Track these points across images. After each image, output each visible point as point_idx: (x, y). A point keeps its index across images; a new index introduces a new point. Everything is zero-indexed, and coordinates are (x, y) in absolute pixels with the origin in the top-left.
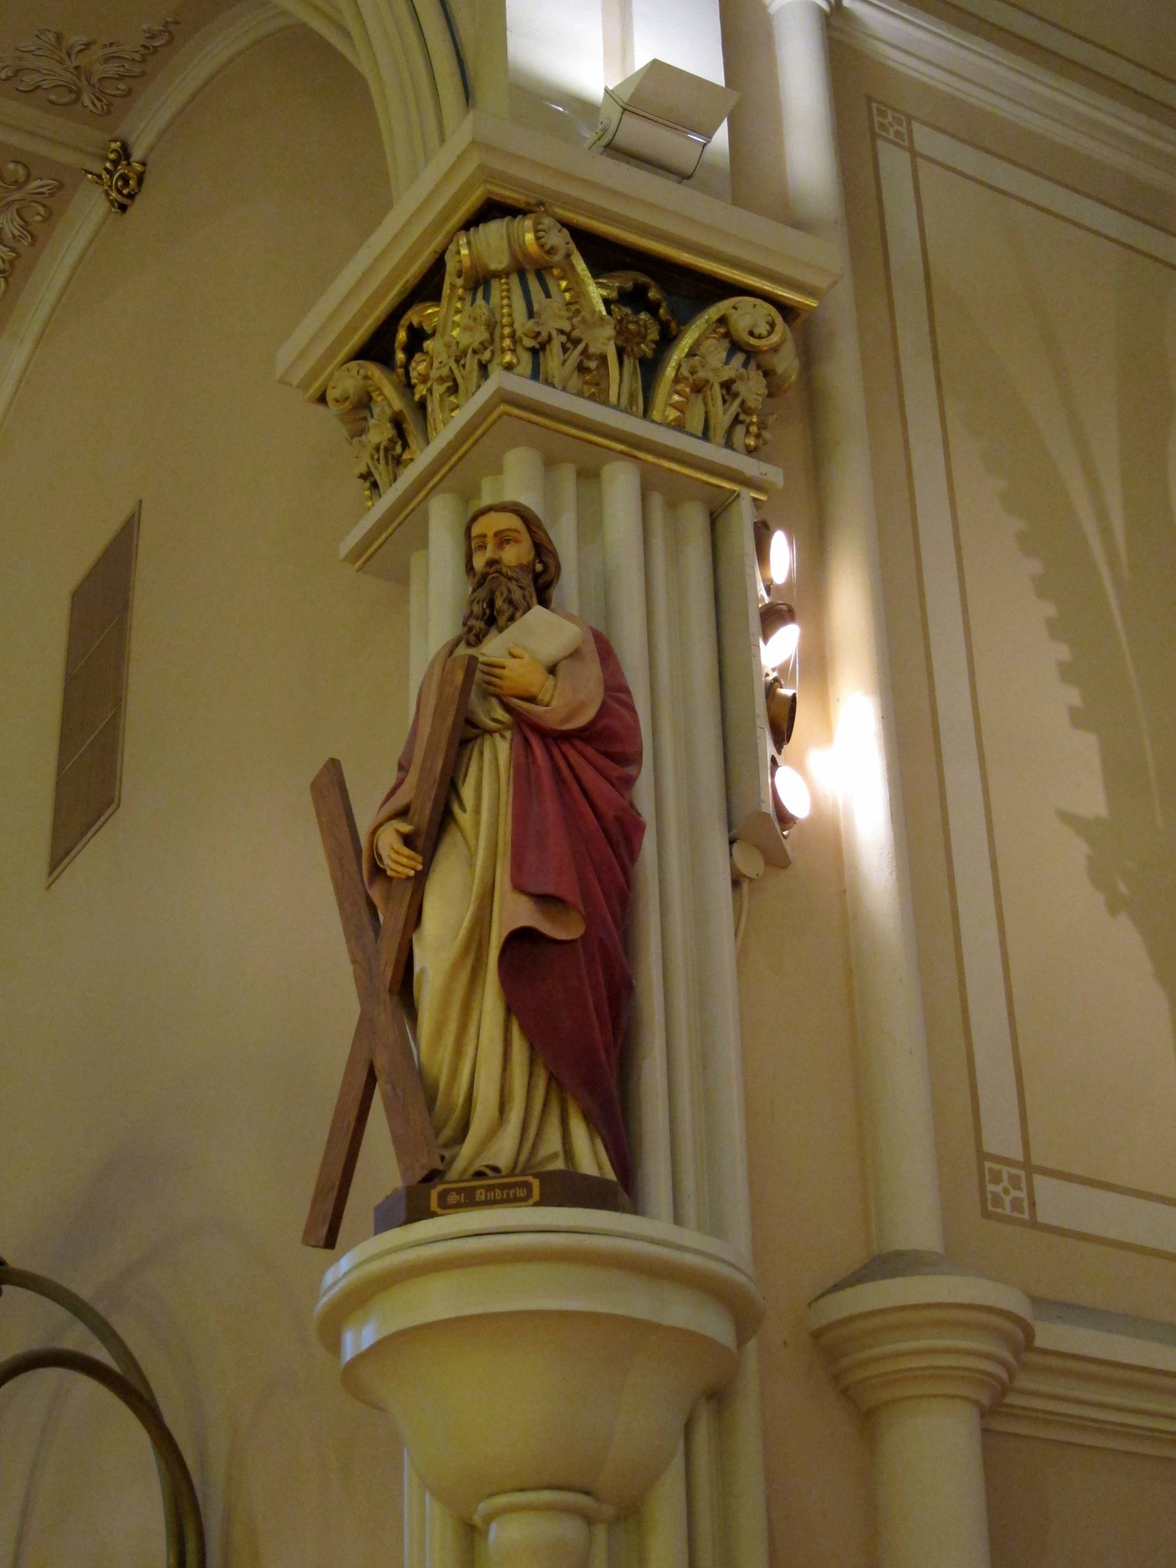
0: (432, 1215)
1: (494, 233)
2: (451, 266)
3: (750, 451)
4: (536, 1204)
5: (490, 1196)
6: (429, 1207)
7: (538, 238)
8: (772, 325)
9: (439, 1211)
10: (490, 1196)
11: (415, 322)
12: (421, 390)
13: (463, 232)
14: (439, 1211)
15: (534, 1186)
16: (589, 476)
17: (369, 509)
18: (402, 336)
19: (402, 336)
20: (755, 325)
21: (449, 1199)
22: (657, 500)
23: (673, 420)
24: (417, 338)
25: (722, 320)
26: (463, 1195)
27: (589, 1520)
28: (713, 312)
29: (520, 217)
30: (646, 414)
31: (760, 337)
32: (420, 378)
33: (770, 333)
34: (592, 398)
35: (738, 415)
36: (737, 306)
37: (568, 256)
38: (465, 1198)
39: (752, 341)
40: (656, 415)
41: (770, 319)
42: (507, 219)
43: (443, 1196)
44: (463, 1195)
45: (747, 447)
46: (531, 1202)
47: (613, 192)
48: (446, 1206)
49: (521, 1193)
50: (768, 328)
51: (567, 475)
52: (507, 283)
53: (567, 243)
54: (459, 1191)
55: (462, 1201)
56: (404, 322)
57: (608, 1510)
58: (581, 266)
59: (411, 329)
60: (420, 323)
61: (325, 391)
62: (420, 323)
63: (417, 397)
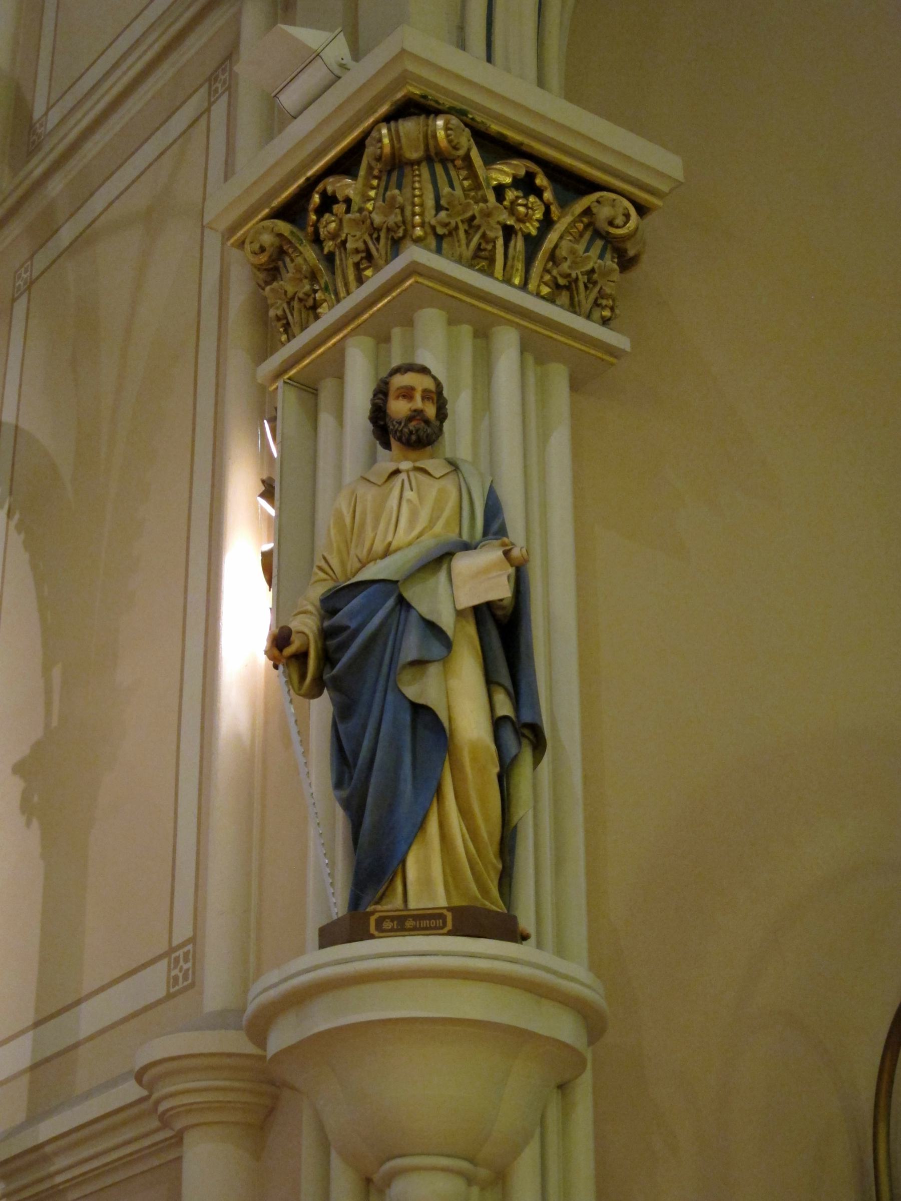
0: (372, 937)
1: (409, 127)
2: (370, 151)
3: (605, 322)
4: (450, 933)
5: (423, 924)
6: (368, 931)
7: (447, 136)
8: (627, 216)
9: (376, 933)
10: (423, 924)
11: (330, 189)
12: (329, 246)
13: (384, 124)
14: (376, 933)
15: (447, 918)
16: (482, 334)
17: (283, 344)
18: (316, 198)
19: (316, 198)
20: (614, 218)
21: (383, 925)
22: (530, 359)
23: (546, 294)
24: (328, 202)
25: (588, 212)
26: (395, 923)
27: (470, 1181)
28: (579, 206)
29: (432, 116)
30: (524, 286)
31: (618, 227)
32: (329, 235)
33: (626, 223)
34: (482, 271)
35: (480, 244)
36: (600, 200)
37: (469, 150)
38: (398, 925)
39: (612, 230)
40: (531, 286)
41: (626, 212)
42: (423, 117)
43: (379, 922)
44: (395, 923)
45: (602, 317)
46: (445, 930)
47: (441, 70)
48: (382, 931)
49: (440, 922)
50: (624, 218)
51: (466, 330)
52: (419, 170)
53: (469, 140)
54: (393, 919)
55: (395, 927)
56: (320, 187)
57: (483, 1173)
58: (475, 155)
59: (324, 194)
60: (334, 192)
61: (245, 239)
62: (334, 192)
63: (326, 251)
